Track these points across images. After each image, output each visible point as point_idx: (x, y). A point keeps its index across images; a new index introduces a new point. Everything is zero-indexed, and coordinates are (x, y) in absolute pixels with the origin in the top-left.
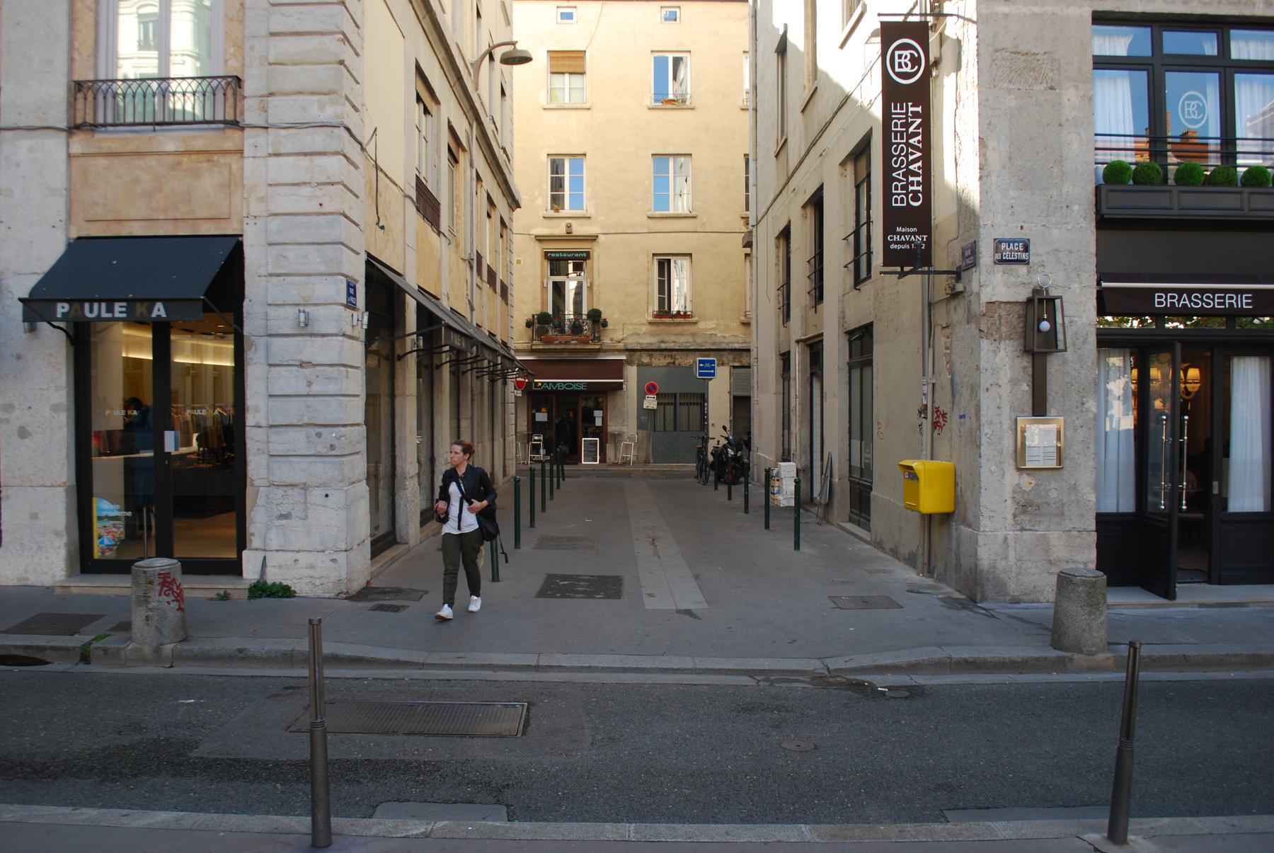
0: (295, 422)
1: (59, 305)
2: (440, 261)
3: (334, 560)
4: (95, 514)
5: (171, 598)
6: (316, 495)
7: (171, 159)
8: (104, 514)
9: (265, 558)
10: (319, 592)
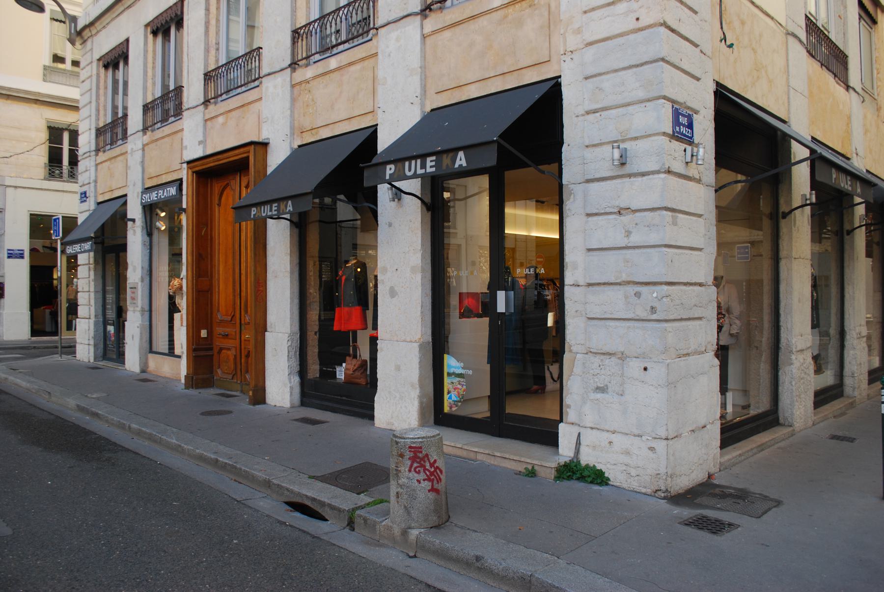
0: (613, 280)
1: (388, 167)
2: (849, 118)
3: (652, 449)
4: (446, 370)
5: (422, 476)
6: (634, 367)
7: (500, 13)
8: (452, 371)
9: (579, 434)
10: (634, 485)
